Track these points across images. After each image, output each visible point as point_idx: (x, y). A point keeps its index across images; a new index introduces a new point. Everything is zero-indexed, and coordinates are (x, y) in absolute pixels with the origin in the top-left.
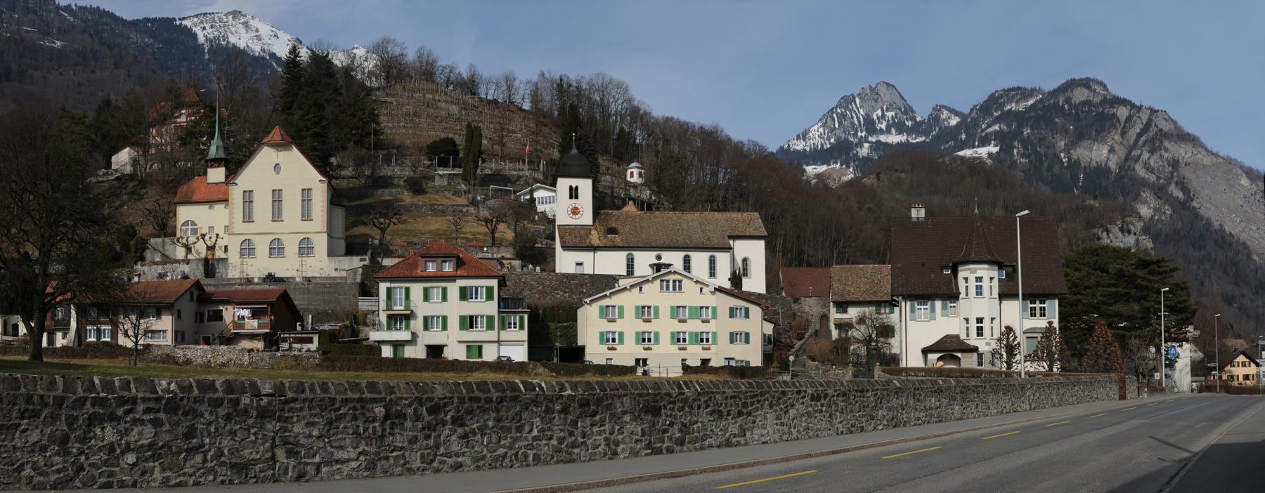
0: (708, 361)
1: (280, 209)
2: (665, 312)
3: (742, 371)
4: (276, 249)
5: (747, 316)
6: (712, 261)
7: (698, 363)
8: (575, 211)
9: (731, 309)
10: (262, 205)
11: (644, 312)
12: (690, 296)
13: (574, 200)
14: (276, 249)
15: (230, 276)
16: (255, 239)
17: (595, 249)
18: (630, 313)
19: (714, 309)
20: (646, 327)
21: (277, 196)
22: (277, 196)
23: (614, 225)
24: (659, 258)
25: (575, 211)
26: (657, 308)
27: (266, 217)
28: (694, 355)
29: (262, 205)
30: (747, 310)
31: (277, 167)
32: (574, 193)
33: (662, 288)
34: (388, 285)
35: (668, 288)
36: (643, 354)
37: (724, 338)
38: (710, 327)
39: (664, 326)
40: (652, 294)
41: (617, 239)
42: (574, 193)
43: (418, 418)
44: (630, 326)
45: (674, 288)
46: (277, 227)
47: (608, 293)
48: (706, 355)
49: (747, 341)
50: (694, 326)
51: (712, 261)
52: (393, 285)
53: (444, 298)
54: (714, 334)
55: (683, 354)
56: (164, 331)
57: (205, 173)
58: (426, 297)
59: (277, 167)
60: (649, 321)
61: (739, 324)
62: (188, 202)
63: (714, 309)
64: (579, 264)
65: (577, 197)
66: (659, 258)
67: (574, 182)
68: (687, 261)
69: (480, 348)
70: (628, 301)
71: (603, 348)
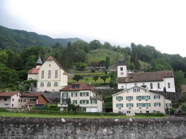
0: (148, 111)
1: (159, 86)
2: (135, 98)
3: (159, 114)
4: (49, 85)
5: (159, 98)
6: (158, 85)
7: (145, 112)
8: (122, 73)
9: (154, 96)
10: (46, 74)
11: (130, 98)
12: (142, 93)
13: (122, 71)
14: (49, 85)
15: (37, 91)
16: (44, 82)
17: (126, 83)
18: (125, 98)
19: (149, 96)
20: (130, 102)
21: (50, 72)
22: (50, 72)
23: (132, 77)
24: (144, 84)
25: (122, 73)
26: (132, 97)
27: (50, 77)
28: (144, 110)
29: (46, 74)
30: (159, 96)
31: (50, 65)
32: (122, 69)
33: (134, 91)
34: (63, 92)
35: (136, 91)
36: (129, 110)
37: (152, 105)
38: (149, 102)
39: (135, 102)
40: (131, 93)
41: (133, 80)
42: (122, 69)
43: (167, 133)
44: (125, 102)
45: (137, 91)
46: (49, 79)
47: (118, 93)
48: (147, 110)
49: (160, 105)
50: (143, 101)
51: (158, 85)
52: (64, 92)
53: (76, 96)
54: (150, 104)
55: (141, 110)
56: (8, 104)
57: (36, 67)
58: (72, 96)
59: (50, 65)
60: (130, 100)
61: (157, 101)
62: (30, 73)
63: (149, 96)
64: (123, 87)
65: (122, 70)
66: (144, 84)
67: (122, 67)
68: (151, 85)
69: (85, 108)
70: (124, 95)
71: (117, 108)
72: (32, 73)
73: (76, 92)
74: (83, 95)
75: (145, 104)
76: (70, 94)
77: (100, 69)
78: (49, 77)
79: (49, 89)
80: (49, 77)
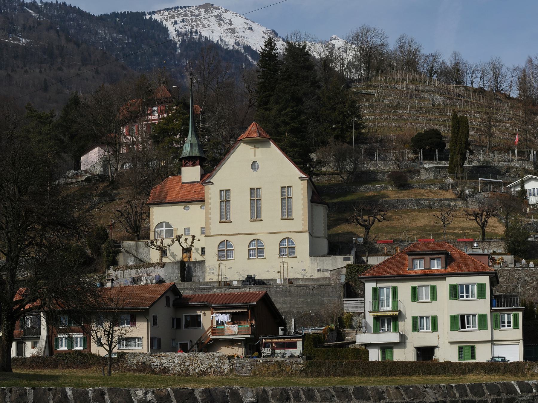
1: (258, 209)
4: (256, 250)
14: (256, 250)
15: (207, 279)
27: (245, 217)
29: (240, 204)
34: (374, 285)
46: (256, 227)
52: (380, 285)
53: (434, 297)
56: (140, 339)
58: (415, 297)
59: (254, 165)
62: (162, 202)
69: (473, 349)
72: (169, 199)
73: (432, 283)
74: (467, 296)
75: (419, 321)
76: (404, 289)
77: (423, 172)
78: (255, 215)
79: (262, 270)
80: (255, 215)
